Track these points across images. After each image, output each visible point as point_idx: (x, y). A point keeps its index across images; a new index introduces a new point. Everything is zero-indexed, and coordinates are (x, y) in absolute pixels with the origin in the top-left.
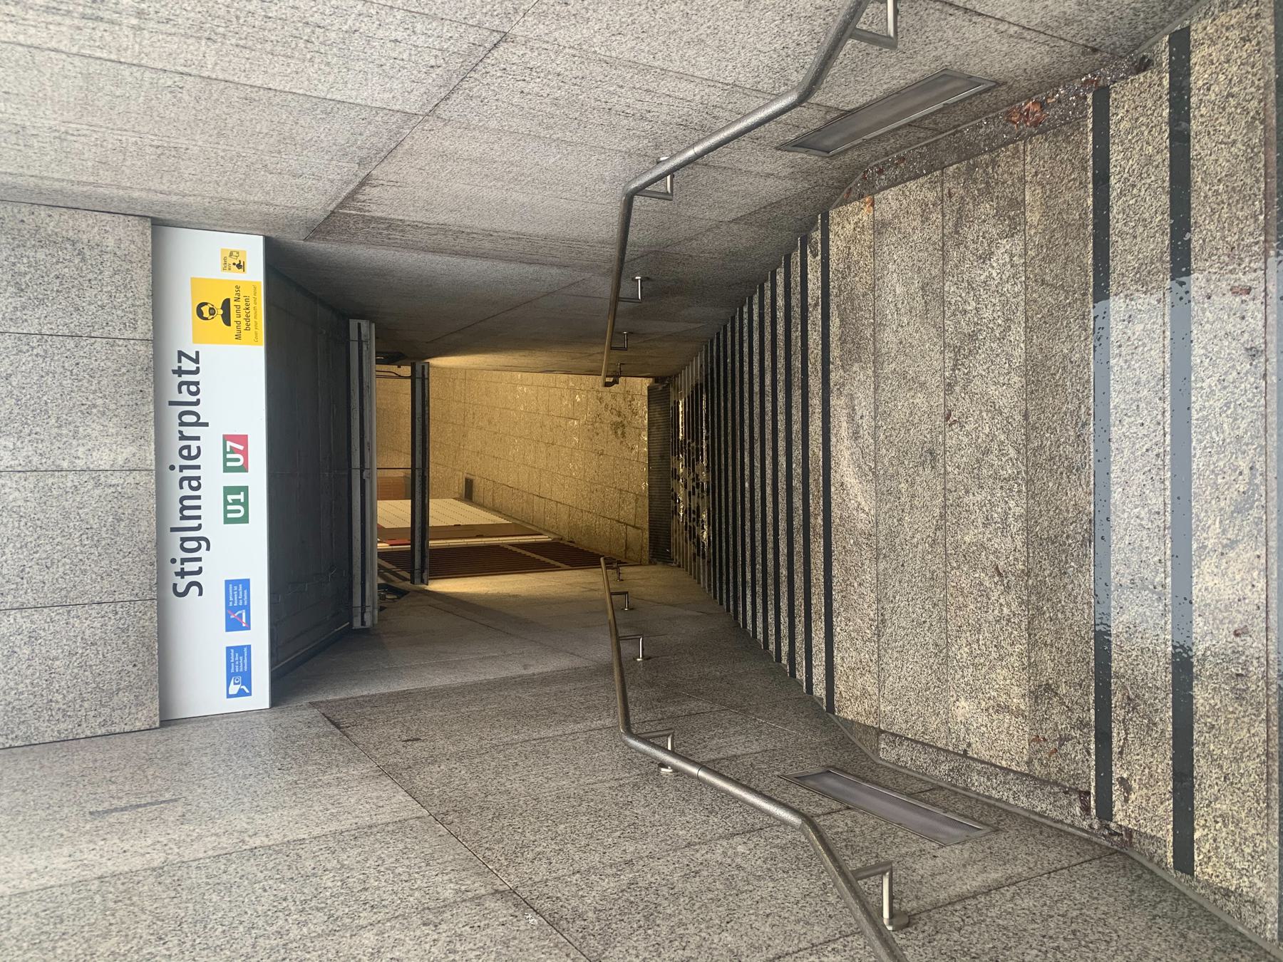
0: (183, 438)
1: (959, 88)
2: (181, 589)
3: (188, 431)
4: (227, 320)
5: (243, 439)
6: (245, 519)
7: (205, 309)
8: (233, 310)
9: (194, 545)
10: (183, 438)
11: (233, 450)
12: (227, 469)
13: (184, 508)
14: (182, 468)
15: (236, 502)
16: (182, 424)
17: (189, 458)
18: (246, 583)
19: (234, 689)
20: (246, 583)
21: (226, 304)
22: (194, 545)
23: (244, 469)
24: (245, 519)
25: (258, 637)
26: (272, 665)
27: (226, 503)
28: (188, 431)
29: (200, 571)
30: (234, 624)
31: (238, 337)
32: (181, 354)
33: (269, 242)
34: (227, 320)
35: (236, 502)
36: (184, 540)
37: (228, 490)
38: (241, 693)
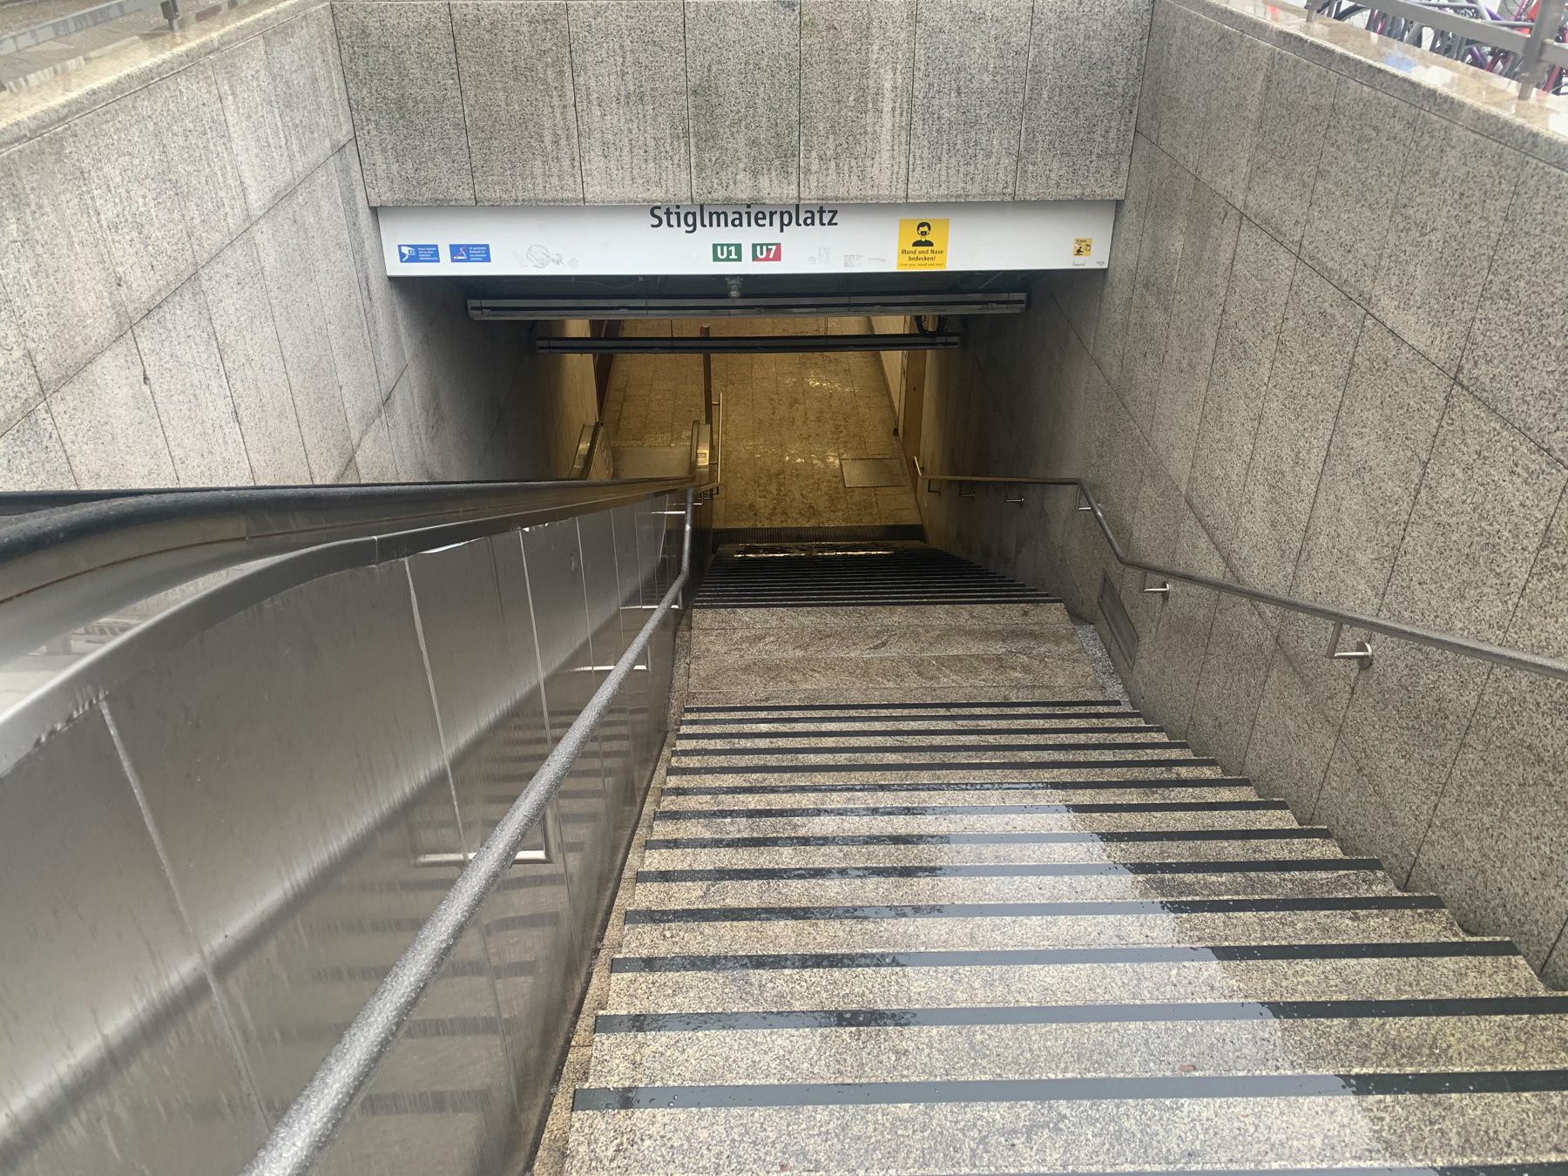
0: (772, 214)
1: (522, 712)
2: (656, 212)
3: (776, 218)
4: (916, 244)
5: (777, 257)
6: (716, 259)
7: (925, 229)
8: (925, 248)
9: (690, 221)
10: (772, 214)
11: (769, 251)
12: (754, 246)
13: (718, 215)
14: (749, 214)
15: (729, 253)
16: (782, 214)
17: (757, 219)
18: (487, 259)
19: (405, 250)
20: (487, 259)
21: (929, 244)
22: (690, 221)
23: (755, 258)
24: (716, 259)
25: (446, 267)
26: (644, 277)
27: (729, 246)
28: (776, 218)
29: (670, 225)
30: (455, 250)
31: (904, 252)
32: (835, 212)
33: (1103, 273)
34: (916, 244)
35: (729, 253)
36: (694, 215)
37: (738, 247)
38: (402, 255)
